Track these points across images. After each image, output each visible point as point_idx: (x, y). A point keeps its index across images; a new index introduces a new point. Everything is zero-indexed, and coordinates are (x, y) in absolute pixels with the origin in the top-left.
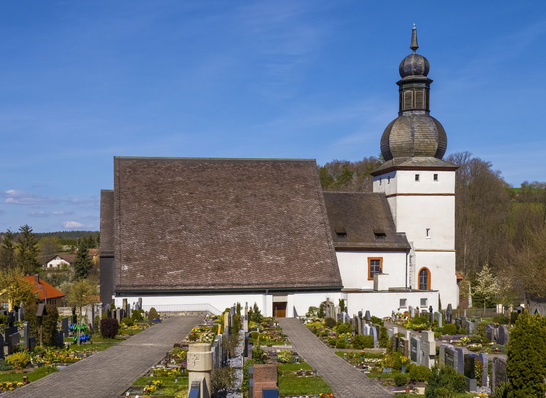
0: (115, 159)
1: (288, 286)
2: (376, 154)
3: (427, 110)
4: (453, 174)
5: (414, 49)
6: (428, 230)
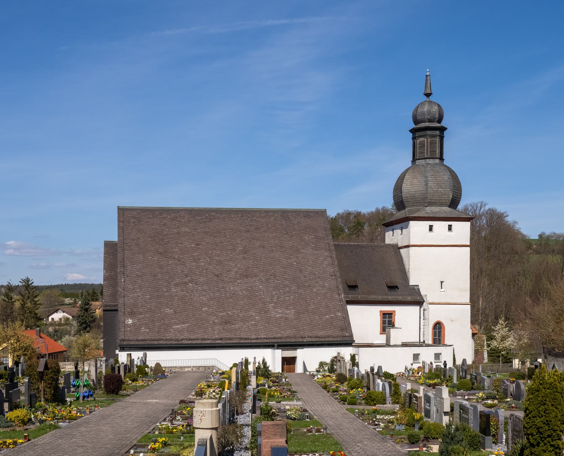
0: (118, 209)
1: (297, 341)
2: (388, 203)
3: (441, 159)
4: (468, 224)
5: (428, 95)
6: (442, 282)
